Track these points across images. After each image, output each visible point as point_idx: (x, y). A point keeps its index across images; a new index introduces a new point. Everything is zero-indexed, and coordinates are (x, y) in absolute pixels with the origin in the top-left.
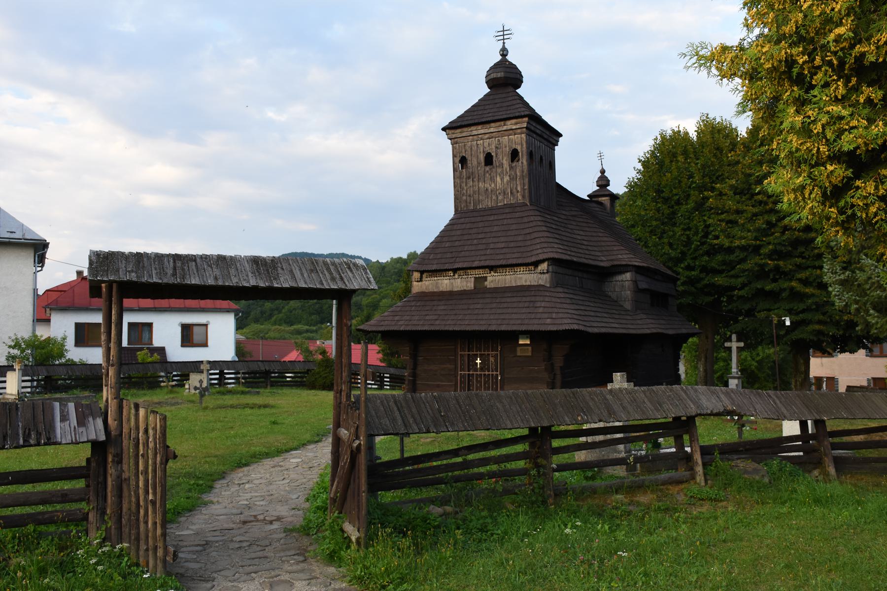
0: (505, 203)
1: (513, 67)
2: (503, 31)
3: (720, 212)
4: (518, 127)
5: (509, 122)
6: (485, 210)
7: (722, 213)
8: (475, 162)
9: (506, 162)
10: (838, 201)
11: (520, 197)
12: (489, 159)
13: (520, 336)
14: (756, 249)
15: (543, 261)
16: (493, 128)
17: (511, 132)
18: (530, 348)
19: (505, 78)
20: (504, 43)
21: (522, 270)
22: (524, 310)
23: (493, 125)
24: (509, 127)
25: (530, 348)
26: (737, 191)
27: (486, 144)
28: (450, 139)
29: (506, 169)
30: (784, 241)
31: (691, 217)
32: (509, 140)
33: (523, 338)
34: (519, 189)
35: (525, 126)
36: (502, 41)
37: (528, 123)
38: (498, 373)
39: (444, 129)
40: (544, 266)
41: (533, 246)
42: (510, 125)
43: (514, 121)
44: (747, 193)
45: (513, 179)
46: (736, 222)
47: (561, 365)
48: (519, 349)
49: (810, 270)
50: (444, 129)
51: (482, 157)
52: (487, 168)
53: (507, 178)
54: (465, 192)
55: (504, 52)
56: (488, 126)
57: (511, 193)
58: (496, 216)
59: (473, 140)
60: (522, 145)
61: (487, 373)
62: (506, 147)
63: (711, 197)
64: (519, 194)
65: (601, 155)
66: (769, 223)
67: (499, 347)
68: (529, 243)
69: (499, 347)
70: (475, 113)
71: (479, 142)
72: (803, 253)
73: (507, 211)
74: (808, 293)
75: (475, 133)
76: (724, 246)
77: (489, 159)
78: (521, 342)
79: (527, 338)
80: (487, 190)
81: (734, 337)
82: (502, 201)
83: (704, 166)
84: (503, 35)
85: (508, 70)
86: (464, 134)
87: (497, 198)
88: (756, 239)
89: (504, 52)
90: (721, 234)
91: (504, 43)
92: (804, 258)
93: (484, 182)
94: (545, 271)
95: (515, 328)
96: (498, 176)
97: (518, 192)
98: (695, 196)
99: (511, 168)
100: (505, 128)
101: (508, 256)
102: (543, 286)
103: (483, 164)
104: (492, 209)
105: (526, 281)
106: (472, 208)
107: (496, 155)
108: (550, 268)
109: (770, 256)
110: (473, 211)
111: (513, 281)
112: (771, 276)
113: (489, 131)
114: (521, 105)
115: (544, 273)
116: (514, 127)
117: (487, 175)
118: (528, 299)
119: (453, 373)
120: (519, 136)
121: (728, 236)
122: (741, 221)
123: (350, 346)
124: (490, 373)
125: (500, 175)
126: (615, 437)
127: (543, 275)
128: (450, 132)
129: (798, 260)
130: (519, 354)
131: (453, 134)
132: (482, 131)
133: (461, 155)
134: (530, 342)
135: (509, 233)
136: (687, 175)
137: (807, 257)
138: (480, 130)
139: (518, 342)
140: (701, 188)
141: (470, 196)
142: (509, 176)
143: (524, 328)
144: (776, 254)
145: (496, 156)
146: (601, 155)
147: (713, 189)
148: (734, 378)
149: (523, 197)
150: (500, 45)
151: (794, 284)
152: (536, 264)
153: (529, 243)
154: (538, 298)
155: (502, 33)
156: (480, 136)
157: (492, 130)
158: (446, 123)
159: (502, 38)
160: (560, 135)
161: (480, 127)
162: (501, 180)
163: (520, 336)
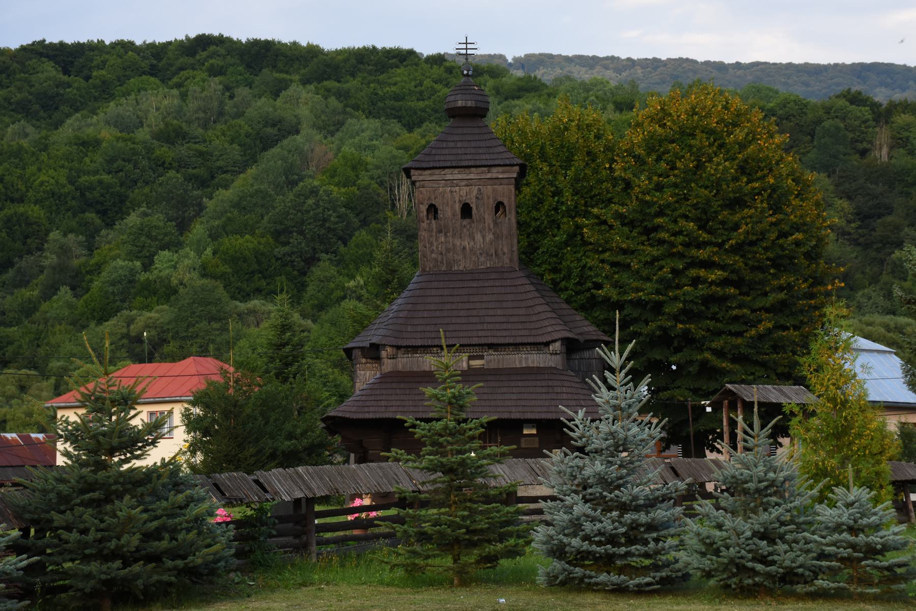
0: (488, 266)
2: (466, 43)
3: (600, 249)
4: (505, 176)
5: (494, 170)
6: (462, 273)
7: (603, 252)
8: (449, 213)
9: (489, 218)
10: (577, 170)
11: (507, 261)
12: (466, 211)
13: (524, 425)
14: (657, 308)
15: (554, 341)
16: (473, 175)
17: (496, 181)
18: (537, 439)
19: (476, 108)
21: (529, 349)
22: (544, 396)
23: (473, 170)
24: (494, 176)
25: (537, 439)
26: (627, 222)
27: (463, 193)
29: (489, 225)
30: (697, 297)
31: (560, 255)
32: (494, 190)
33: (528, 428)
34: (506, 250)
35: (515, 176)
41: (541, 322)
42: (496, 173)
43: (500, 169)
44: (639, 226)
45: (497, 237)
46: (628, 266)
48: (523, 440)
49: (724, 336)
51: (458, 207)
52: (465, 222)
53: (489, 237)
54: (435, 248)
56: (467, 170)
57: (496, 254)
58: (480, 282)
59: (446, 186)
60: (510, 198)
62: (488, 198)
63: (587, 226)
64: (505, 257)
66: (674, 271)
68: (534, 318)
71: (454, 189)
72: (716, 313)
73: (493, 276)
74: (724, 368)
75: (449, 177)
76: (612, 300)
77: (466, 211)
78: (525, 432)
79: (533, 427)
80: (464, 248)
82: (485, 263)
83: (577, 180)
84: (466, 49)
85: (480, 98)
86: (434, 178)
87: (478, 259)
88: (658, 292)
90: (605, 281)
92: (717, 320)
93: (461, 238)
94: (558, 352)
96: (479, 233)
97: (504, 254)
98: (567, 225)
99: (496, 223)
100: (489, 176)
101: (514, 333)
102: (555, 368)
103: (459, 216)
104: (471, 272)
105: (533, 362)
106: (444, 268)
107: (477, 207)
109: (676, 318)
110: (445, 273)
111: (517, 362)
112: (676, 344)
113: (468, 177)
115: (556, 354)
116: (501, 176)
117: (465, 230)
118: (544, 383)
120: (506, 187)
121: (616, 285)
122: (635, 266)
125: (481, 232)
127: (553, 356)
129: (711, 324)
130: (523, 446)
131: (421, 175)
132: (460, 177)
133: (430, 202)
134: (537, 431)
135: (505, 305)
136: (551, 191)
137: (721, 319)
138: (456, 175)
139: (522, 431)
140: (573, 213)
141: (441, 254)
142: (493, 234)
143: (529, 416)
144: (687, 315)
145: (477, 208)
147: (586, 215)
149: (511, 260)
151: (707, 355)
152: (547, 344)
153: (534, 318)
154: (555, 383)
155: (464, 46)
156: (455, 182)
157: (472, 176)
161: (456, 171)
162: (483, 238)
163: (524, 425)
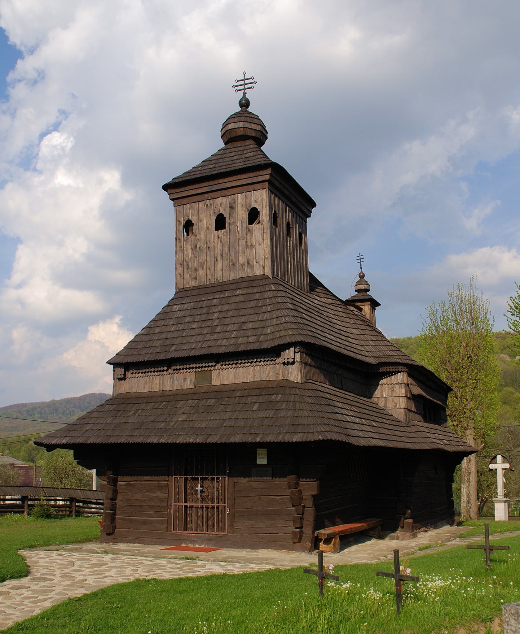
1: (255, 119)
15: (287, 346)
20: (245, 93)
28: (172, 200)
36: (243, 91)
37: (271, 175)
38: (226, 505)
39: (166, 187)
40: (289, 354)
47: (315, 493)
50: (166, 187)
55: (245, 104)
61: (210, 505)
65: (360, 258)
67: (228, 468)
69: (228, 468)
70: (206, 167)
81: (499, 458)
89: (245, 104)
91: (245, 93)
95: (250, 439)
108: (298, 356)
114: (262, 156)
119: (165, 504)
123: (486, 544)
124: (215, 505)
126: (303, 209)
128: (173, 191)
146: (360, 258)
148: (500, 502)
150: (240, 94)
158: (168, 180)
159: (242, 87)
160: (313, 205)
